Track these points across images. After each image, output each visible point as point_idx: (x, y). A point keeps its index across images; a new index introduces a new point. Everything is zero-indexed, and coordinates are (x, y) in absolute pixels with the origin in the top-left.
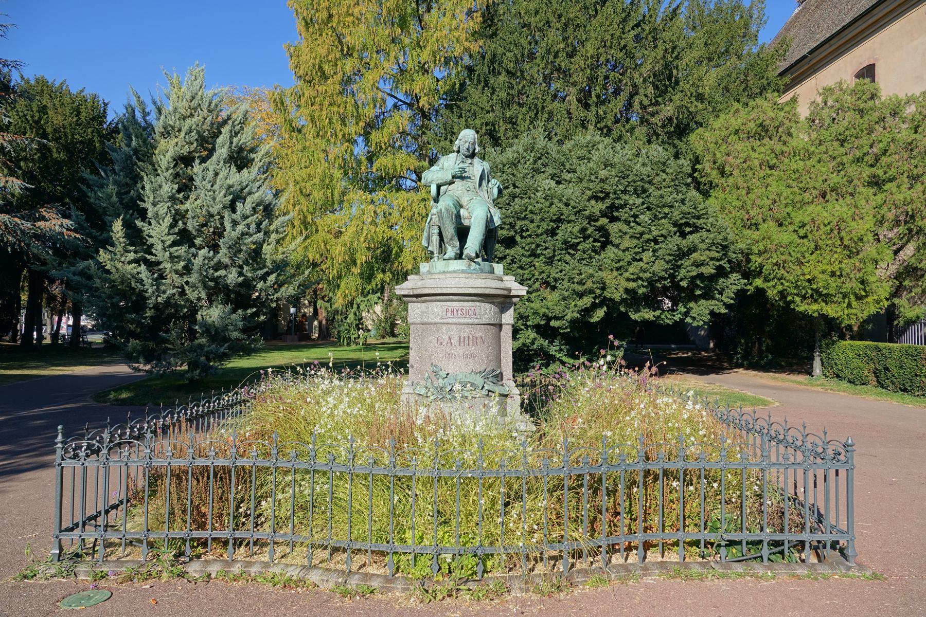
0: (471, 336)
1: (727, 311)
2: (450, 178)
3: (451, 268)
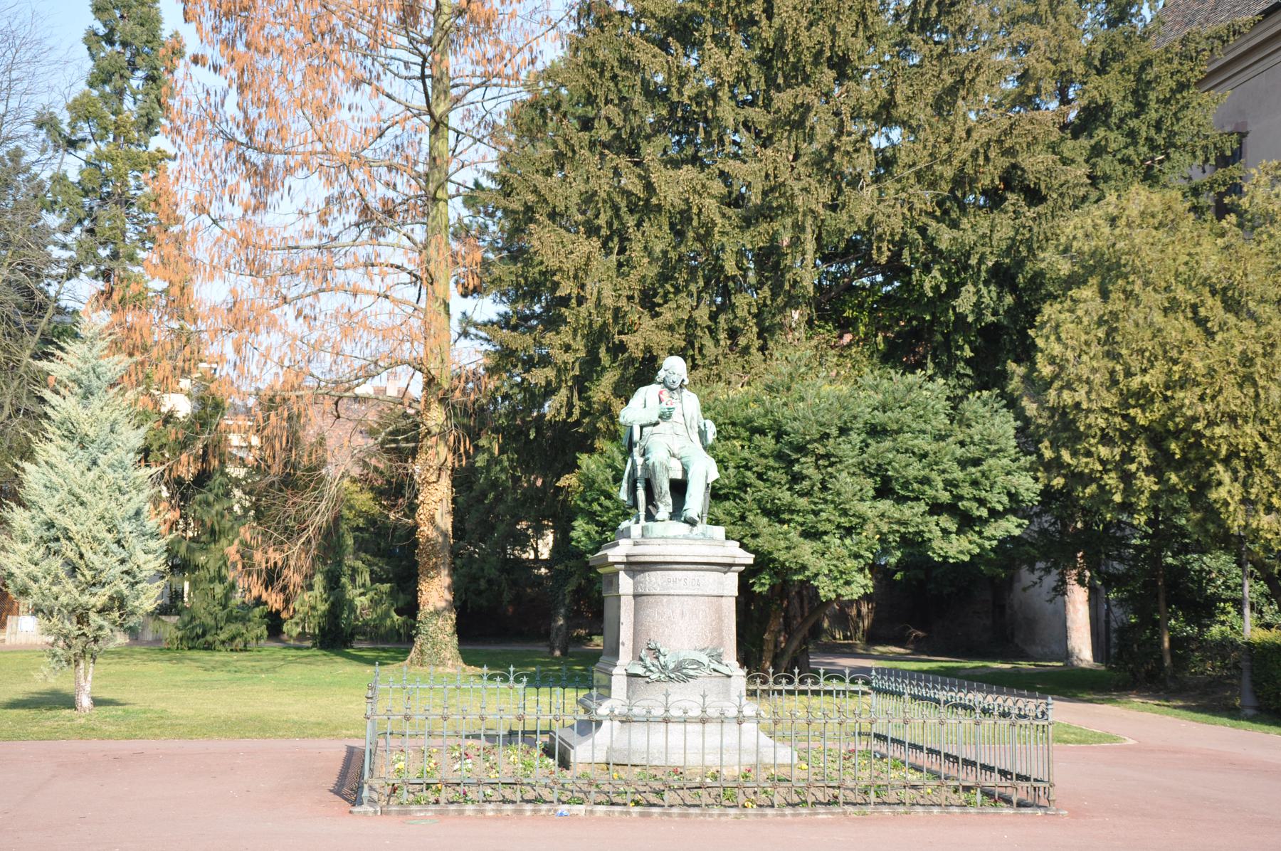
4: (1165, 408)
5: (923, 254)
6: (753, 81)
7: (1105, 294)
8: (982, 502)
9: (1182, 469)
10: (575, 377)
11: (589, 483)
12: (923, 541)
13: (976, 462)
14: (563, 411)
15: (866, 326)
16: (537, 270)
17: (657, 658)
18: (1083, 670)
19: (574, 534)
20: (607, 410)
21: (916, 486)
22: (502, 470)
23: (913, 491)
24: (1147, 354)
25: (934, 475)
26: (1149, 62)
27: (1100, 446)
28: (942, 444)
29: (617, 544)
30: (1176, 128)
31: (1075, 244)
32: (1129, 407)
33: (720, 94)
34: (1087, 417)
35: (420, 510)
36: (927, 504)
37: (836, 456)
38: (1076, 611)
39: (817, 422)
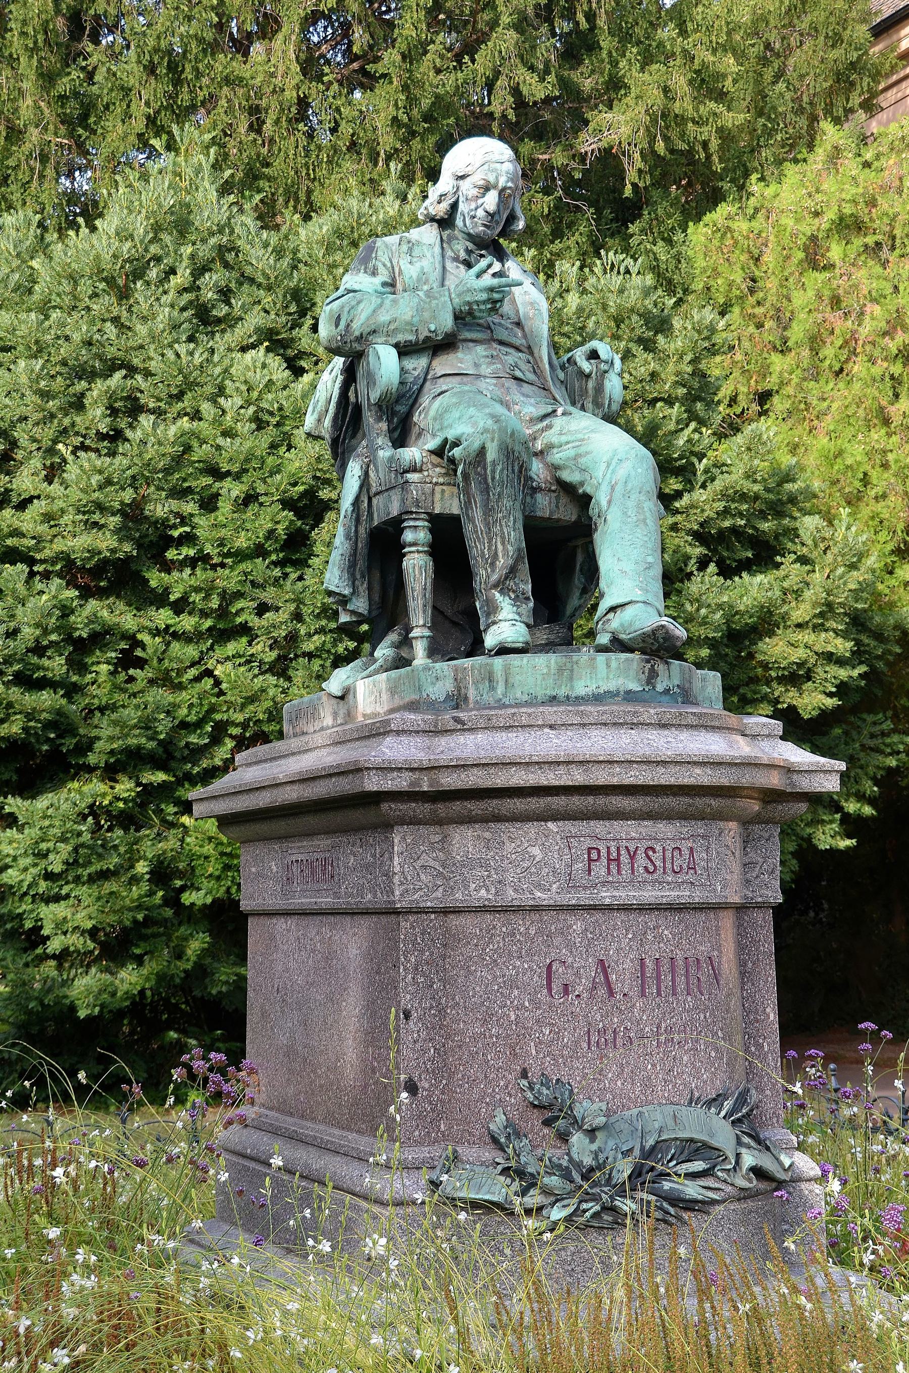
0: (679, 955)
1: (845, 843)
2: (446, 323)
3: (582, 687)
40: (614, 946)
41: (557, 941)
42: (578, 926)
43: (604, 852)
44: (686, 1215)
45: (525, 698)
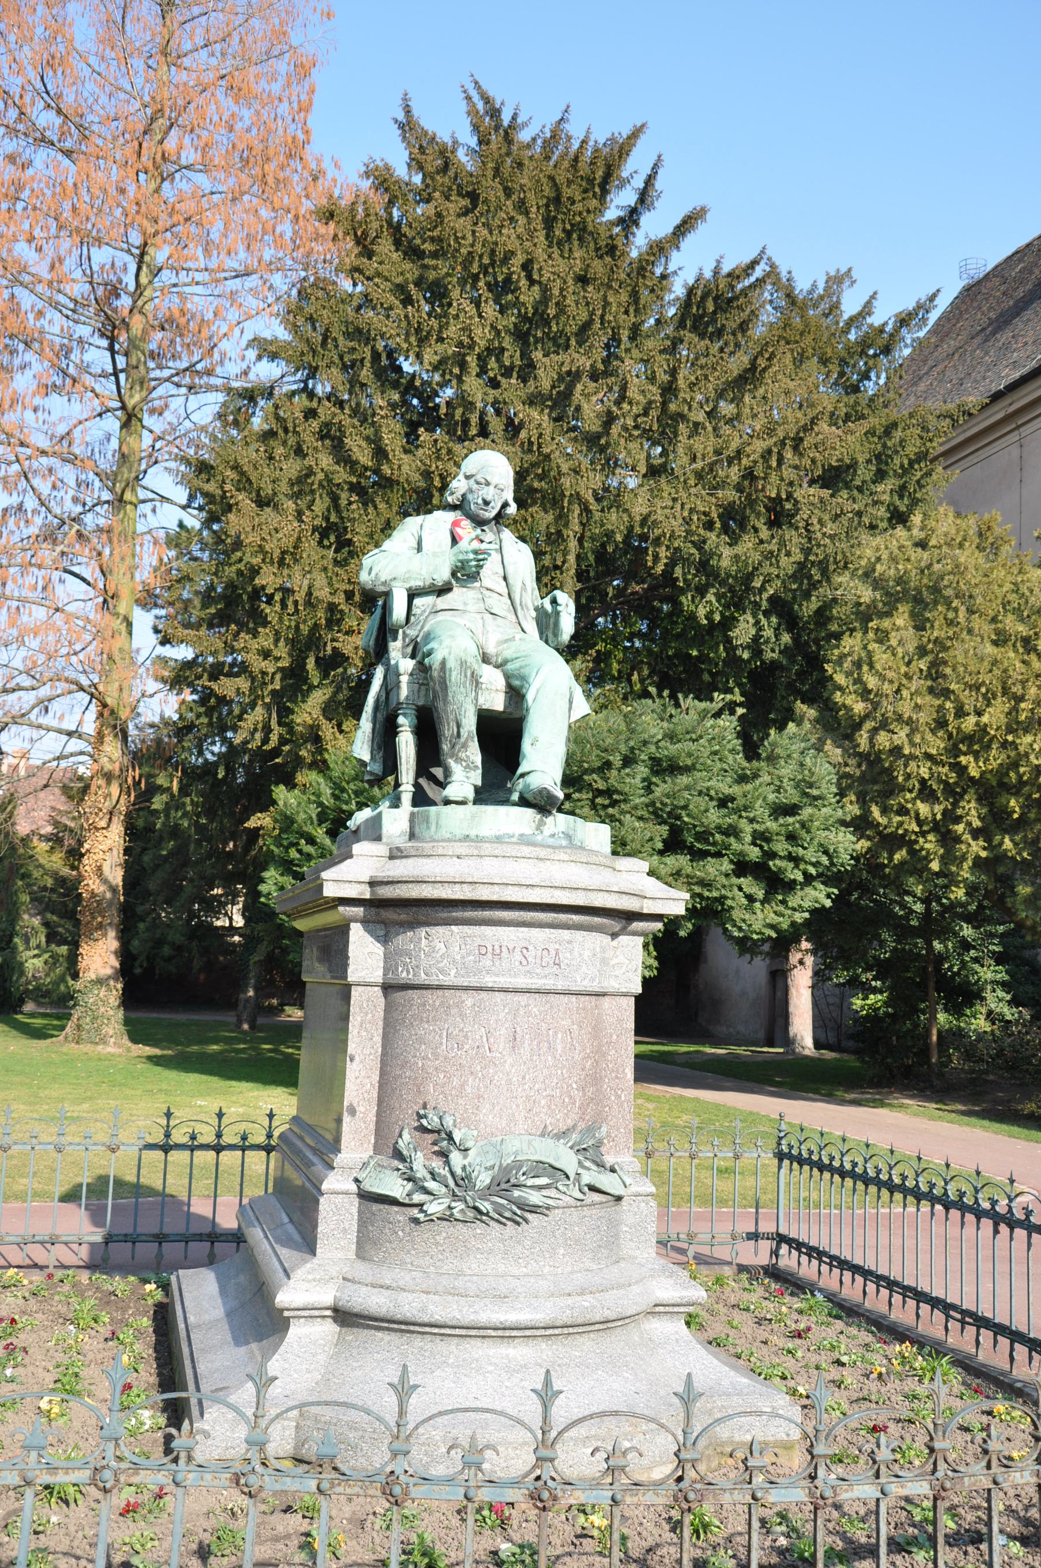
4: (1003, 756)
5: (695, 576)
6: (506, 354)
7: (920, 625)
8: (796, 860)
9: (1016, 833)
10: (274, 692)
11: (287, 822)
12: (723, 910)
13: (791, 810)
14: (258, 736)
15: (619, 663)
16: (234, 568)
17: (444, 1155)
18: (807, 1057)
19: (263, 888)
20: (315, 737)
21: (718, 837)
22: (185, 814)
23: (714, 844)
24: (983, 690)
25: (744, 824)
26: (894, 425)
27: (918, 802)
28: (749, 787)
29: (349, 856)
30: (918, 495)
31: (878, 567)
32: (959, 753)
33: (469, 359)
34: (906, 766)
35: (85, 860)
36: (731, 861)
37: (620, 793)
38: (800, 995)
39: (598, 746)
40: (494, 1018)
41: (454, 1011)
42: (469, 1002)
43: (490, 949)
44: (528, 1215)
45: (448, 836)
